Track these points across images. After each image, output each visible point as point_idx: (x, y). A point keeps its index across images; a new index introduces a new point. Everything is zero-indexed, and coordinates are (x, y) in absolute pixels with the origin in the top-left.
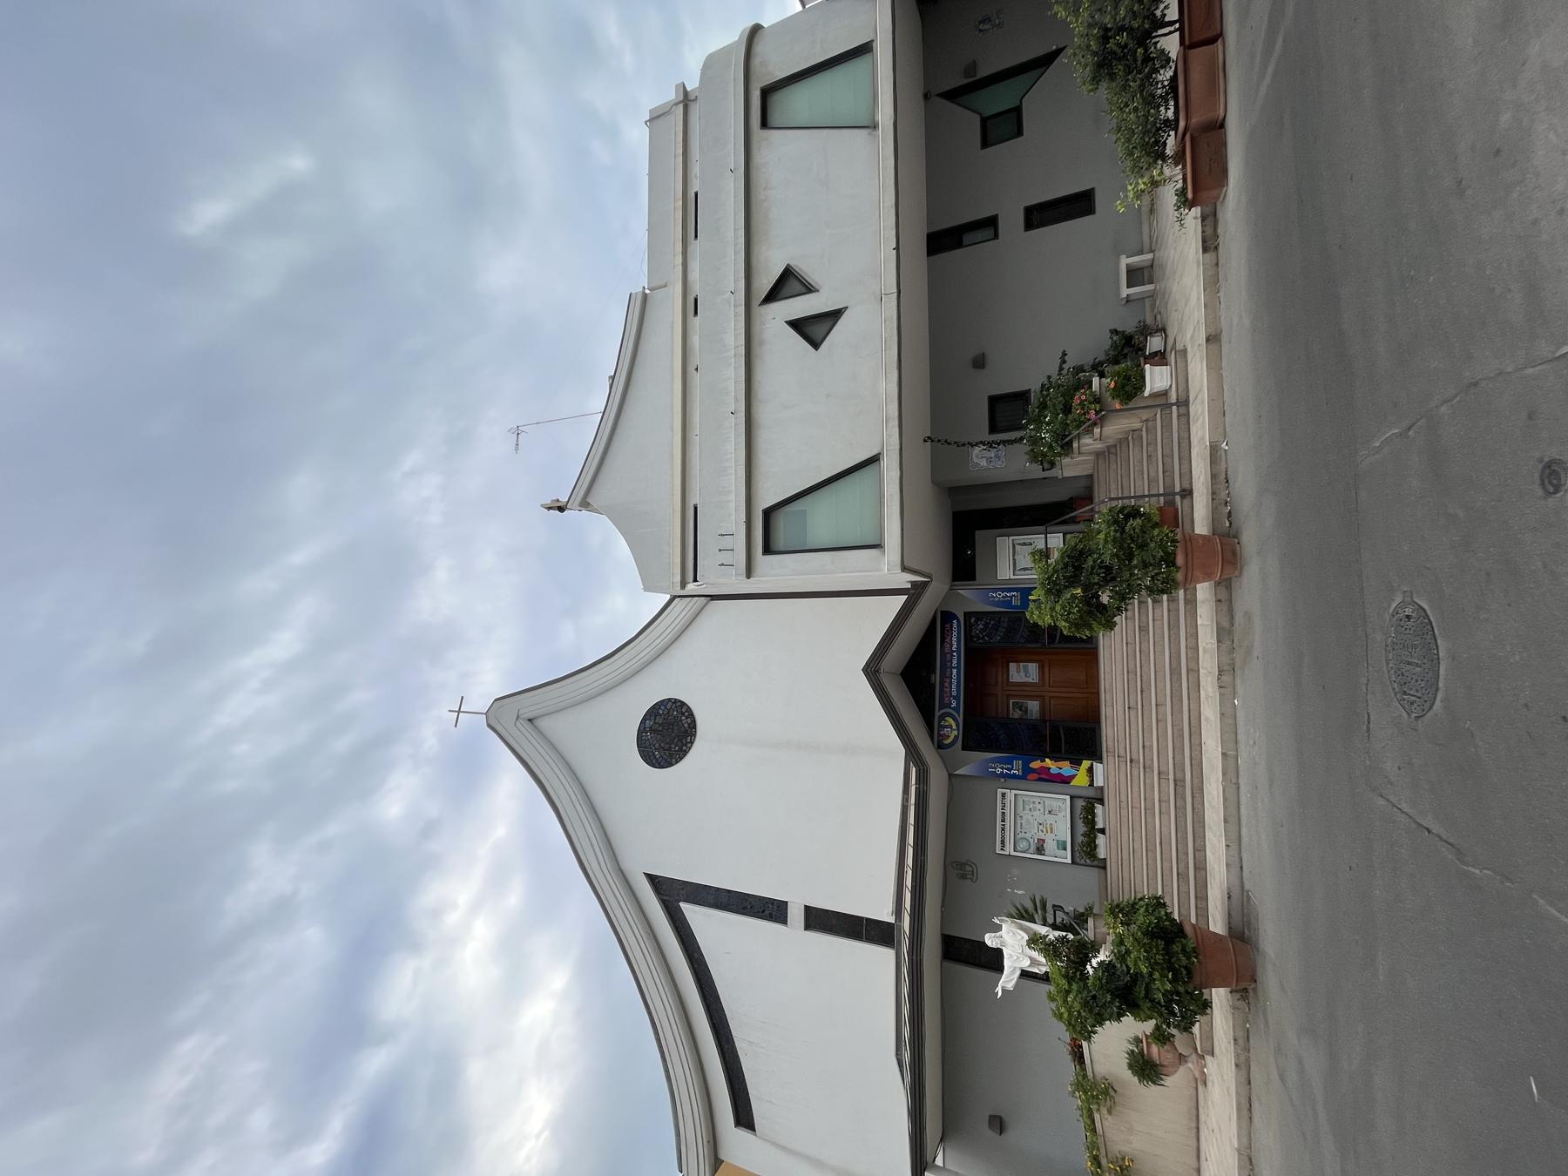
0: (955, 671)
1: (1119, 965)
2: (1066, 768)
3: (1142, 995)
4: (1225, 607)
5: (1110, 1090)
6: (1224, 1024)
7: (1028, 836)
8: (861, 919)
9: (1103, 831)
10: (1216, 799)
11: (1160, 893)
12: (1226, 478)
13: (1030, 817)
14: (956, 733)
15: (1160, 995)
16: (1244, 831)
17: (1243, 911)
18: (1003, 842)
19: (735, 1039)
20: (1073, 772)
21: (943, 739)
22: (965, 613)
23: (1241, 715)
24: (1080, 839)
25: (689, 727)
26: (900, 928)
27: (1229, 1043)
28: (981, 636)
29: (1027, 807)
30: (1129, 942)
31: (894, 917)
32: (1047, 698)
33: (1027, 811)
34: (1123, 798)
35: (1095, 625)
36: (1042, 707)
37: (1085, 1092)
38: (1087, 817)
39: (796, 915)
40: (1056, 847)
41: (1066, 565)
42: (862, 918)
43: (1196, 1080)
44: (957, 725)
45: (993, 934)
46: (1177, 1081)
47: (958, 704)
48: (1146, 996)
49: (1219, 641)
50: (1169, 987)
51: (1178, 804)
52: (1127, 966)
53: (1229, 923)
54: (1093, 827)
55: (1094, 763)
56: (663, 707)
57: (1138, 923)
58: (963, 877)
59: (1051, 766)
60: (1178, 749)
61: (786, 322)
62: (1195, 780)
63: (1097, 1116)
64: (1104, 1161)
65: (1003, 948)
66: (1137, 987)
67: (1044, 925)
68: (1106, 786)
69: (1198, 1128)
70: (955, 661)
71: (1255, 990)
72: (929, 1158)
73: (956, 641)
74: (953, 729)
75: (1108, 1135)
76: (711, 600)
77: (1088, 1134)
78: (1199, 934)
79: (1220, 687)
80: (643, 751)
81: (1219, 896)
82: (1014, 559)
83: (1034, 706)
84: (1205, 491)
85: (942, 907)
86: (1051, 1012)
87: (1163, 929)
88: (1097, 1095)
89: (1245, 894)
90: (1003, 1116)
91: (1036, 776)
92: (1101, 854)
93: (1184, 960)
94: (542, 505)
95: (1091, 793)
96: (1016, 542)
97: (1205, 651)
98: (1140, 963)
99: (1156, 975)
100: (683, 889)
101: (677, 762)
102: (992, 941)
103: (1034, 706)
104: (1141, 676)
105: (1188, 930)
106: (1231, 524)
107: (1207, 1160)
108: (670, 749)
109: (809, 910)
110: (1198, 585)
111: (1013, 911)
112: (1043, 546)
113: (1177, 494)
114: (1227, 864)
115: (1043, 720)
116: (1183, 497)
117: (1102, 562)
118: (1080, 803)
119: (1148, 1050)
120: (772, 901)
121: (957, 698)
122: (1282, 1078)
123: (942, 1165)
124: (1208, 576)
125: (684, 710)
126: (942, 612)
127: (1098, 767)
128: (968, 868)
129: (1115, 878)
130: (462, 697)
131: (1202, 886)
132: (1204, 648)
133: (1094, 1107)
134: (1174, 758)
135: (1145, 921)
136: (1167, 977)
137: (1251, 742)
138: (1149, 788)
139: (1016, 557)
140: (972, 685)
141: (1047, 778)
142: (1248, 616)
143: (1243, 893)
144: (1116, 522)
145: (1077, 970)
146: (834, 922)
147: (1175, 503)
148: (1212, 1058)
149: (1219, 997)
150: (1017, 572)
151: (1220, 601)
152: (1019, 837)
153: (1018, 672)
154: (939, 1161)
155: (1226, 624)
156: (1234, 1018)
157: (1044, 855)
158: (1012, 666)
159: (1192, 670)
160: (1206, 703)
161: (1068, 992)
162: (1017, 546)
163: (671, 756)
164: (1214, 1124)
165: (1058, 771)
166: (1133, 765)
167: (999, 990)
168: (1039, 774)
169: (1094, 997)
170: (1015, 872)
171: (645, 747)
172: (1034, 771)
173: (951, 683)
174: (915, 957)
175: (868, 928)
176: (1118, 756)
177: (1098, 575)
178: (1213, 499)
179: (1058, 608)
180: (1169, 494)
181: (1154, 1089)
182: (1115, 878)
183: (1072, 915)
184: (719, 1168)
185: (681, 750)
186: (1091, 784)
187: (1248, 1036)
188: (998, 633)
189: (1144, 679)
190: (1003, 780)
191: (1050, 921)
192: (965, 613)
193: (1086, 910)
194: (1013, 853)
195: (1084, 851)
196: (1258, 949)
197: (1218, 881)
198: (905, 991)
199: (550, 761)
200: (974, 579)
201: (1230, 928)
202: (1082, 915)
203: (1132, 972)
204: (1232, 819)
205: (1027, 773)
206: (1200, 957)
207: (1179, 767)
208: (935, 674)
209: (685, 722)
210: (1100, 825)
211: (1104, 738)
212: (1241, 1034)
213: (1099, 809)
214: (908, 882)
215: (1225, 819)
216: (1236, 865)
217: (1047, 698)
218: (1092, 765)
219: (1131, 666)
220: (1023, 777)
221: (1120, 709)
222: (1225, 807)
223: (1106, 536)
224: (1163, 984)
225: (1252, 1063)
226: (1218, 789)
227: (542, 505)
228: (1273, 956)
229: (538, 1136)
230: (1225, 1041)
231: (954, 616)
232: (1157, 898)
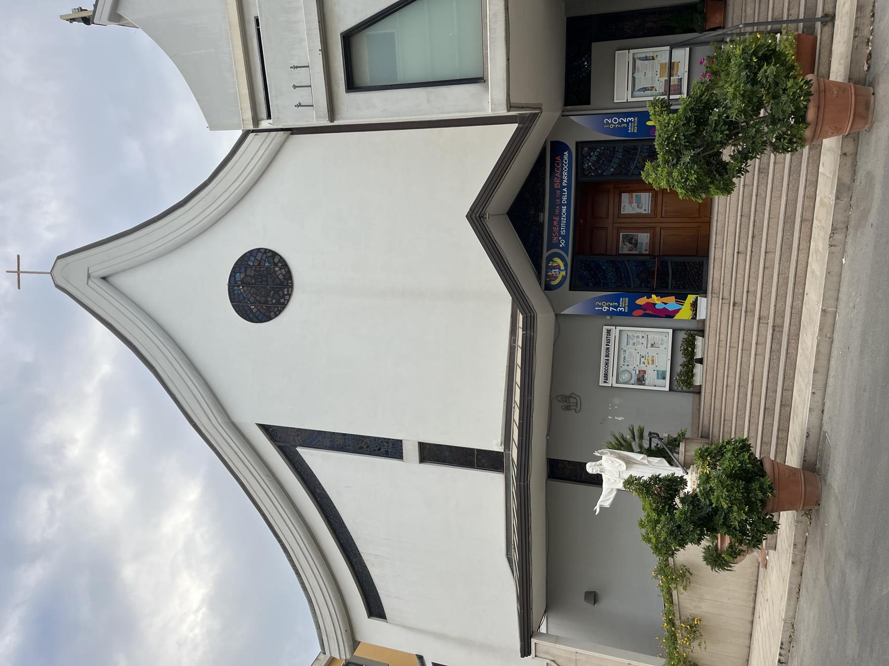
0: (564, 209)
1: (703, 500)
2: (671, 303)
3: (721, 522)
4: (849, 161)
5: (687, 574)
6: (788, 530)
7: (631, 368)
8: (471, 450)
9: (701, 361)
10: (809, 350)
11: (745, 436)
12: (873, 11)
13: (632, 351)
14: (564, 273)
15: (736, 523)
16: (831, 381)
17: (818, 447)
18: (606, 376)
19: (362, 554)
20: (677, 307)
21: (550, 280)
22: (577, 143)
23: (846, 276)
24: (679, 369)
25: (284, 278)
26: (509, 456)
27: (790, 546)
28: (593, 168)
29: (631, 342)
30: (713, 484)
31: (503, 447)
32: (658, 230)
33: (630, 345)
34: (723, 337)
35: (712, 188)
36: (652, 239)
37: (666, 576)
38: (687, 349)
39: (411, 451)
40: (656, 378)
41: (688, 120)
42: (474, 449)
43: (759, 563)
44: (566, 265)
45: (594, 463)
46: (745, 564)
47: (567, 244)
48: (724, 524)
49: (837, 198)
50: (744, 517)
51: (774, 347)
52: (710, 500)
53: (804, 457)
54: (692, 358)
55: (699, 298)
56: (252, 259)
57: (724, 466)
58: (568, 408)
59: (657, 302)
60: (781, 297)
62: (793, 328)
63: (674, 593)
64: (677, 622)
65: (603, 474)
66: (717, 516)
67: (641, 453)
68: (708, 318)
69: (756, 594)
70: (565, 198)
71: (817, 511)
72: (535, 628)
73: (567, 176)
74: (560, 269)
75: (682, 604)
76: (292, 134)
77: (666, 604)
78: (776, 471)
79: (831, 246)
80: (238, 306)
81: (799, 432)
82: (634, 78)
83: (644, 238)
84: (848, 22)
85: (548, 435)
86: (641, 536)
87: (746, 471)
88: (676, 579)
89: (822, 433)
90: (595, 591)
91: (641, 312)
92: (697, 381)
93: (760, 495)
94: (61, 17)
95: (693, 325)
96: (637, 56)
97: (822, 204)
98: (722, 500)
99: (735, 508)
100: (298, 435)
101: (276, 316)
102: (592, 469)
103: (644, 238)
104: (754, 221)
105: (767, 467)
106: (869, 68)
107: (759, 618)
108: (266, 302)
109: (422, 446)
110: (824, 140)
111: (614, 441)
112: (667, 61)
113: (818, 20)
114: (810, 409)
115: (652, 255)
116: (824, 24)
117: (727, 117)
118: (682, 336)
119: (721, 547)
120: (387, 440)
121: (566, 237)
122: (828, 579)
123: (545, 632)
124: (837, 131)
125: (276, 260)
126: (552, 143)
127: (702, 302)
128: (572, 400)
129: (708, 405)
130: (19, 288)
131: (784, 429)
132: (821, 199)
133: (673, 586)
134: (775, 305)
135: (730, 466)
136: (744, 510)
137: (851, 304)
138: (748, 330)
139: (636, 75)
140: (582, 221)
141: (652, 313)
142: (870, 176)
143: (820, 432)
144: (748, 66)
145: (666, 504)
146: (447, 454)
147: (814, 28)
148: (774, 551)
149: (786, 520)
150: (636, 93)
151: (845, 154)
152: (621, 369)
153: (631, 203)
154: (543, 629)
155: (847, 180)
156: (796, 530)
157: (644, 385)
158: (624, 196)
159: (806, 220)
160: (814, 255)
161: (658, 522)
162: (637, 60)
163: (269, 309)
164: (769, 595)
165: (663, 306)
166: (736, 308)
167: (597, 508)
168: (645, 310)
169: (679, 527)
170: (617, 401)
171: (240, 302)
172: (640, 307)
173: (560, 222)
174: (522, 483)
175: (480, 457)
176: (722, 299)
177: (722, 132)
178: (855, 37)
179: (675, 174)
180: (809, 21)
181: (723, 574)
182: (708, 405)
183: (666, 441)
184: (356, 649)
185: (278, 302)
186: (694, 316)
187: (806, 542)
188: (612, 164)
189: (757, 224)
190: (609, 317)
191: (646, 445)
192: (577, 143)
193: (679, 436)
194: (615, 385)
195: (681, 380)
196: (825, 481)
197: (800, 420)
198: (514, 505)
199: (139, 323)
200: (589, 103)
201: (804, 461)
202: (675, 440)
203: (714, 506)
204: (822, 370)
205: (633, 308)
206: (775, 492)
207: (779, 314)
209: (280, 273)
210: (698, 356)
211: (710, 280)
212: (801, 540)
213: (699, 341)
214: (517, 398)
215: (815, 370)
216: (819, 409)
217: (658, 230)
218: (696, 300)
219: (746, 210)
220: (629, 314)
221: (730, 251)
222: (817, 359)
223: (735, 89)
224: (739, 515)
225: (805, 562)
226: (812, 342)
227: (61, 17)
228: (837, 491)
229: (198, 610)
230: (787, 544)
231: (565, 147)
232: (743, 441)
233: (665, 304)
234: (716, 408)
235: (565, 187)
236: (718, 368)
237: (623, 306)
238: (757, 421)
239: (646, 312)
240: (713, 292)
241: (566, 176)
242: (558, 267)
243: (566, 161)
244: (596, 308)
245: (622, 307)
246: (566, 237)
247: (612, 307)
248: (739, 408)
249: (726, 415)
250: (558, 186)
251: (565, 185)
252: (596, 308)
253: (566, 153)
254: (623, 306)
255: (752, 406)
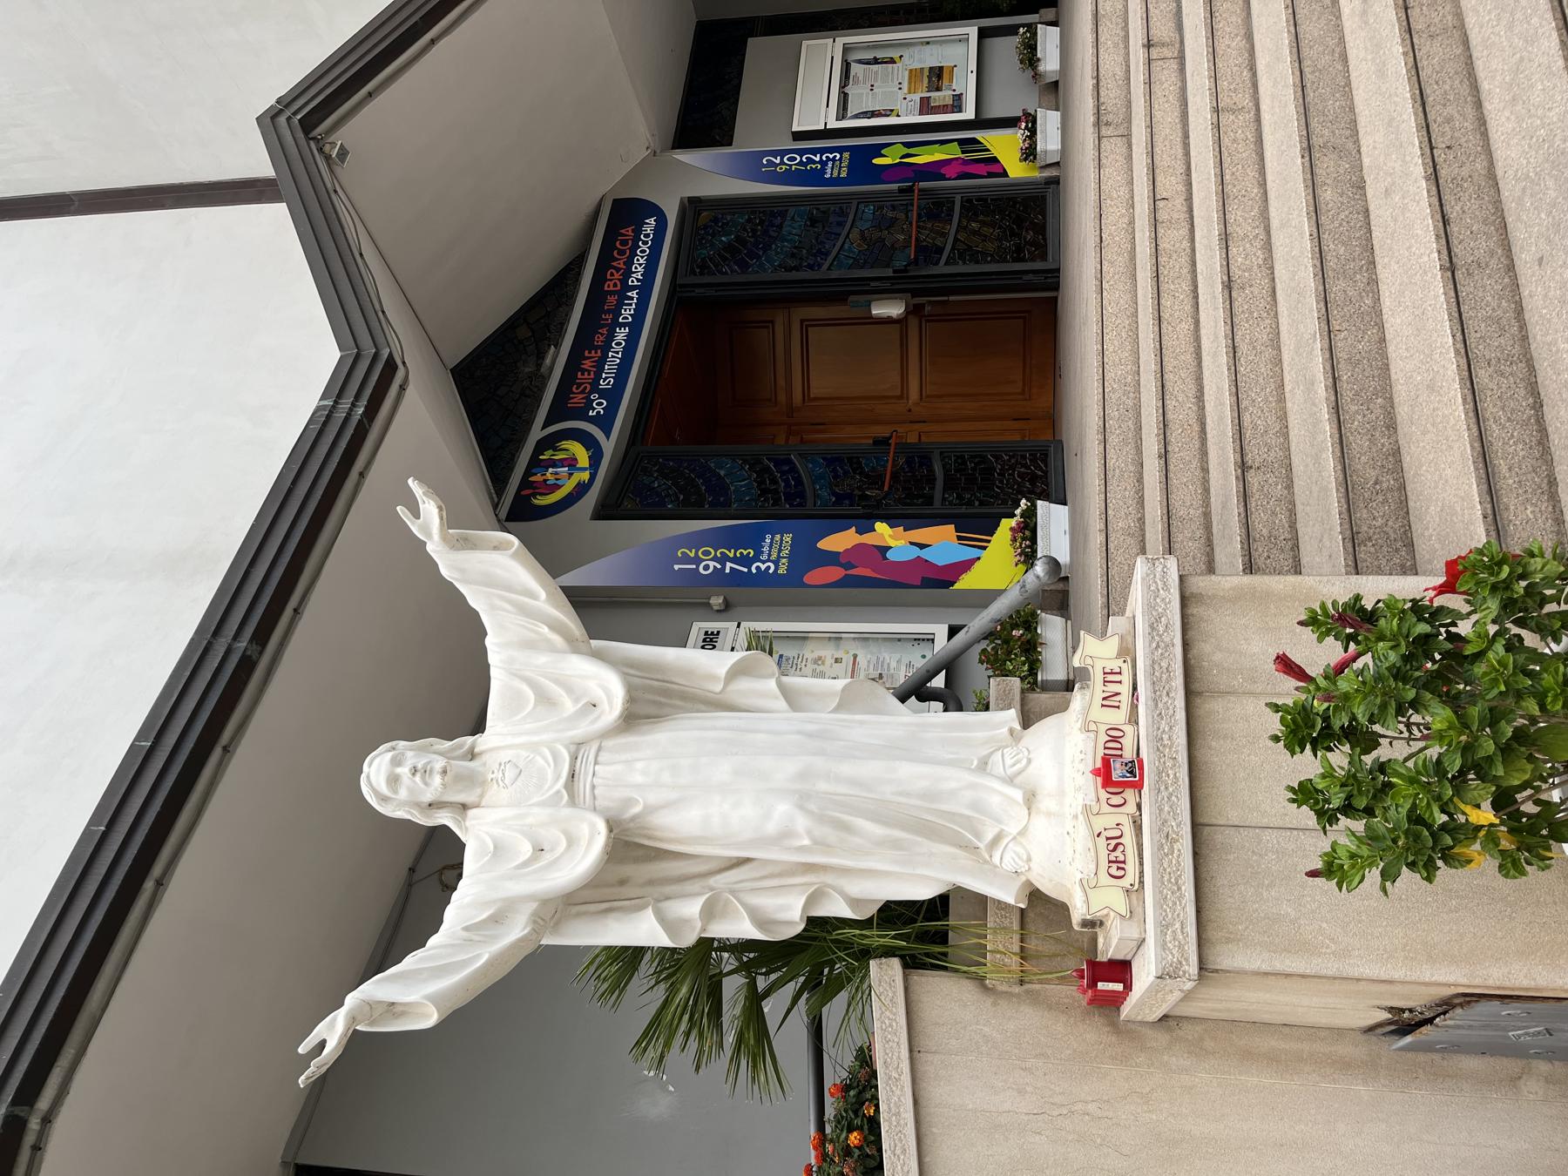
0: (621, 335)
2: (942, 543)
14: (586, 476)
59: (891, 543)
61: (560, 587)
70: (627, 313)
162: (853, 65)
165: (915, 553)
172: (832, 558)
208: (558, 345)
218: (1034, 506)
233: (922, 546)
234: (1180, 511)
235: (633, 288)
236: (1165, 315)
237: (774, 557)
238: (1480, 165)
239: (850, 572)
240: (1104, 119)
241: (640, 265)
242: (571, 463)
243: (647, 236)
244: (676, 567)
245: (769, 560)
246: (614, 396)
247: (734, 560)
248: (1331, 263)
249: (1248, 434)
250: (615, 285)
251: (636, 283)
252: (676, 567)
253: (652, 221)
254: (774, 557)
255: (1428, 91)
